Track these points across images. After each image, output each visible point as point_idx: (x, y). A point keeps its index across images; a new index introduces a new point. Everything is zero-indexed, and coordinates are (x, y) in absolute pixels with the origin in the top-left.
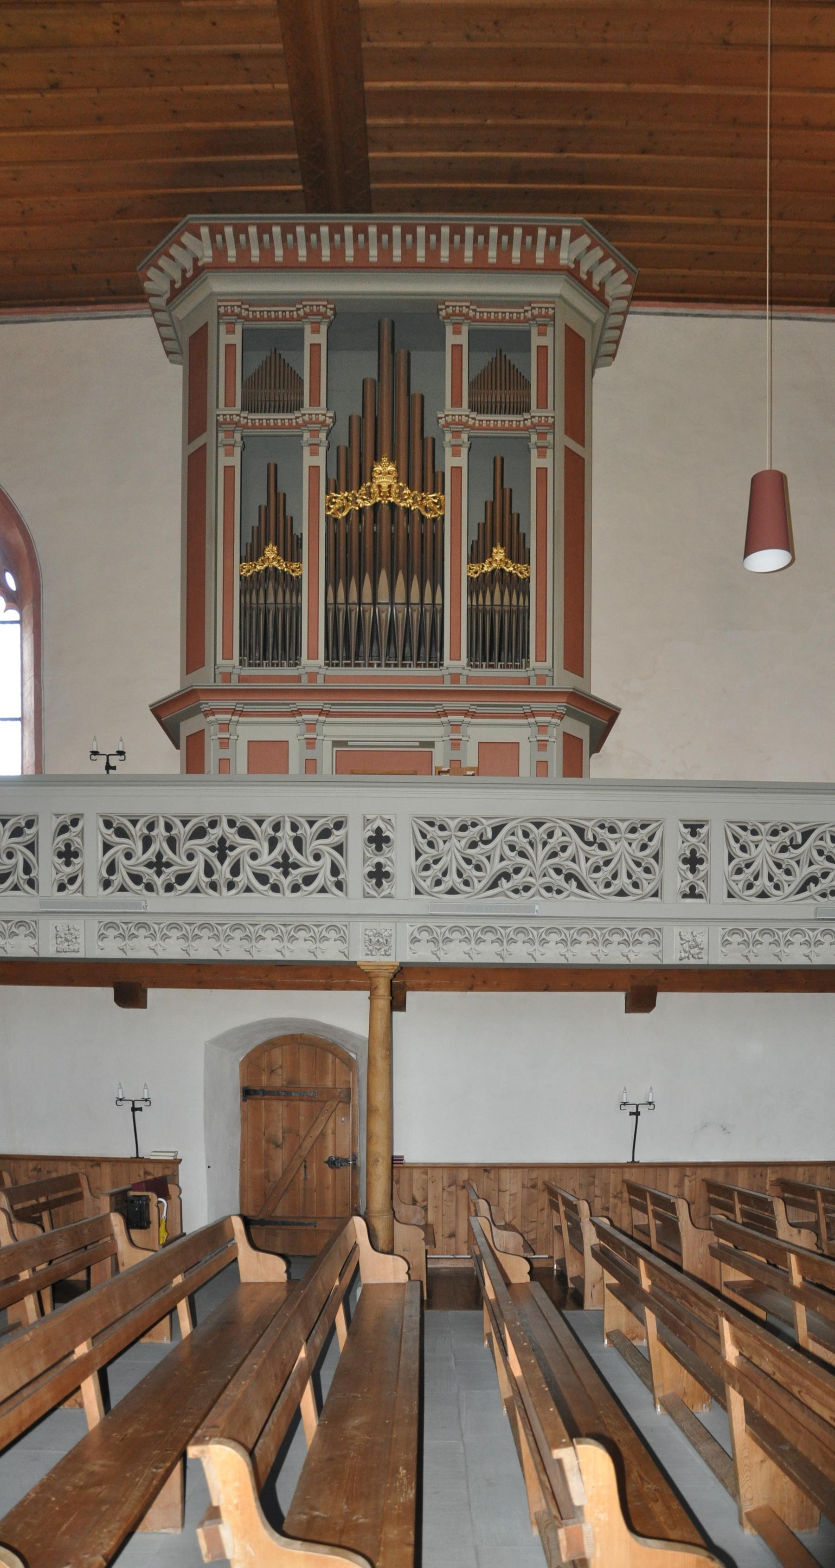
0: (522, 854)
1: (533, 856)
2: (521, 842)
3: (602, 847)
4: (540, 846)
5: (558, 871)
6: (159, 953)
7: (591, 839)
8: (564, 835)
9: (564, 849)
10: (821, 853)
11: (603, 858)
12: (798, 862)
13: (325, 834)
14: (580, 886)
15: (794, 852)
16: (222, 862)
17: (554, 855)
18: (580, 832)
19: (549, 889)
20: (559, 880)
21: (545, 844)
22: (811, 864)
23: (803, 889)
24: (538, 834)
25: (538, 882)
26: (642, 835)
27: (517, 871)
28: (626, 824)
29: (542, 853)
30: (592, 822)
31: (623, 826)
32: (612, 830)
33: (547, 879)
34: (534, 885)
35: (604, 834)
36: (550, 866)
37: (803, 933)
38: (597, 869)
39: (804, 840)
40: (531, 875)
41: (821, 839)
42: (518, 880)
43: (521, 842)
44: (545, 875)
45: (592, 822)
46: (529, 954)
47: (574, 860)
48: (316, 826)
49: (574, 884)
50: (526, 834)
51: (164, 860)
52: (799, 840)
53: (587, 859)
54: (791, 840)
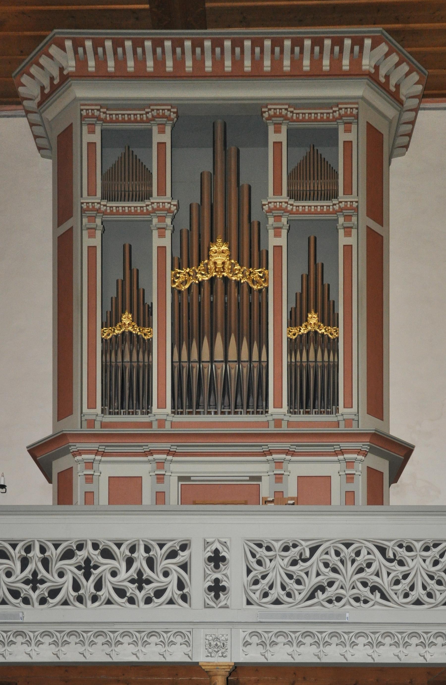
0: (335, 570)
1: (344, 571)
2: (334, 560)
3: (401, 563)
4: (349, 563)
5: (365, 584)
6: (33, 658)
7: (392, 557)
8: (369, 553)
9: (369, 565)
10: (326, 565)
11: (261, 573)
12: (307, 573)
13: (173, 554)
14: (383, 597)
15: (301, 565)
16: (87, 579)
17: (361, 570)
18: (383, 550)
19: (357, 599)
20: (365, 592)
21: (353, 561)
22: (318, 574)
23: (312, 596)
24: (347, 553)
25: (348, 594)
26: (434, 552)
27: (331, 584)
28: (421, 543)
29: (351, 569)
30: (393, 543)
31: (418, 546)
32: (409, 549)
33: (355, 591)
34: (345, 596)
35: (402, 553)
36: (358, 580)
37: (366, 635)
38: (397, 582)
39: (312, 554)
40: (342, 588)
41: (327, 553)
42: (331, 592)
43: (334, 560)
44: (353, 588)
45: (393, 543)
46: (341, 655)
47: (377, 575)
48: (60, 549)
49: (378, 595)
50: (337, 553)
51: (39, 577)
52: (308, 554)
53: (389, 574)
54: (301, 555)
